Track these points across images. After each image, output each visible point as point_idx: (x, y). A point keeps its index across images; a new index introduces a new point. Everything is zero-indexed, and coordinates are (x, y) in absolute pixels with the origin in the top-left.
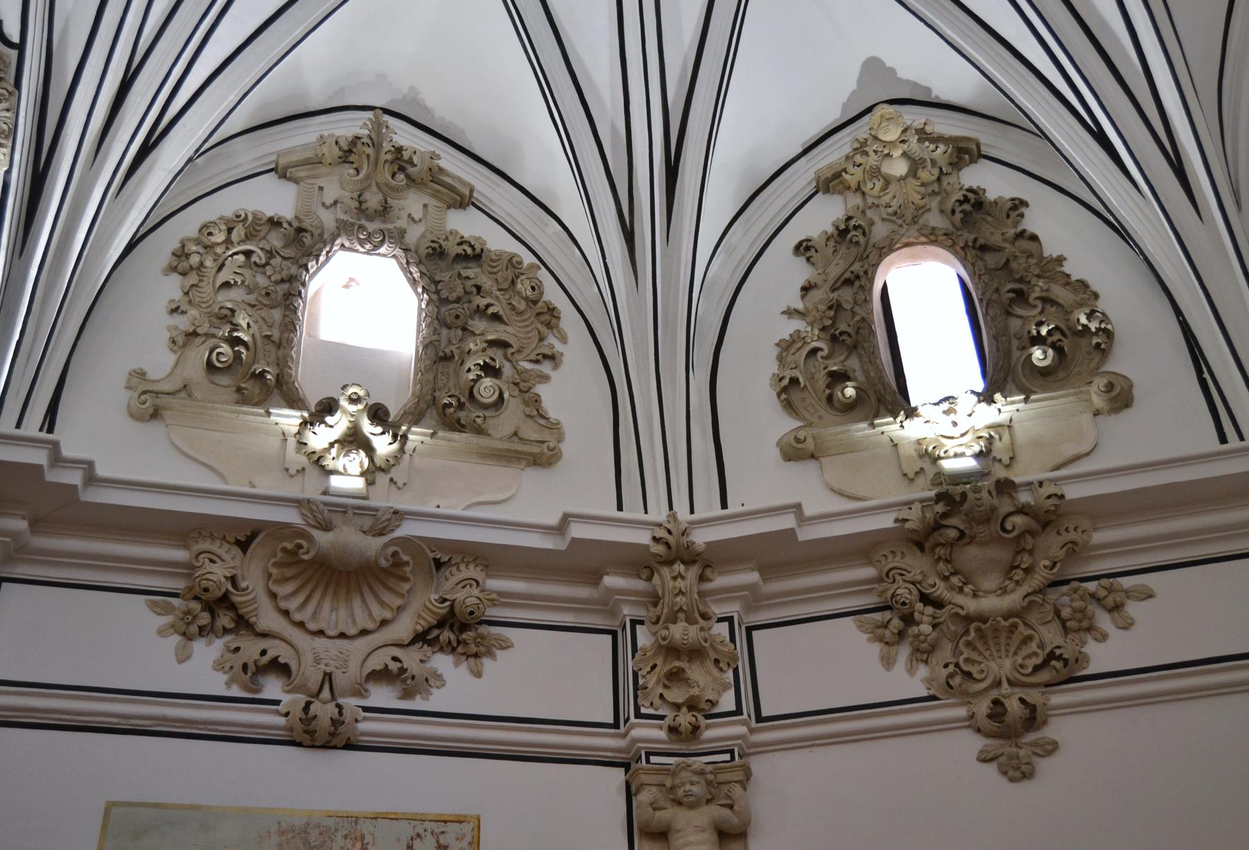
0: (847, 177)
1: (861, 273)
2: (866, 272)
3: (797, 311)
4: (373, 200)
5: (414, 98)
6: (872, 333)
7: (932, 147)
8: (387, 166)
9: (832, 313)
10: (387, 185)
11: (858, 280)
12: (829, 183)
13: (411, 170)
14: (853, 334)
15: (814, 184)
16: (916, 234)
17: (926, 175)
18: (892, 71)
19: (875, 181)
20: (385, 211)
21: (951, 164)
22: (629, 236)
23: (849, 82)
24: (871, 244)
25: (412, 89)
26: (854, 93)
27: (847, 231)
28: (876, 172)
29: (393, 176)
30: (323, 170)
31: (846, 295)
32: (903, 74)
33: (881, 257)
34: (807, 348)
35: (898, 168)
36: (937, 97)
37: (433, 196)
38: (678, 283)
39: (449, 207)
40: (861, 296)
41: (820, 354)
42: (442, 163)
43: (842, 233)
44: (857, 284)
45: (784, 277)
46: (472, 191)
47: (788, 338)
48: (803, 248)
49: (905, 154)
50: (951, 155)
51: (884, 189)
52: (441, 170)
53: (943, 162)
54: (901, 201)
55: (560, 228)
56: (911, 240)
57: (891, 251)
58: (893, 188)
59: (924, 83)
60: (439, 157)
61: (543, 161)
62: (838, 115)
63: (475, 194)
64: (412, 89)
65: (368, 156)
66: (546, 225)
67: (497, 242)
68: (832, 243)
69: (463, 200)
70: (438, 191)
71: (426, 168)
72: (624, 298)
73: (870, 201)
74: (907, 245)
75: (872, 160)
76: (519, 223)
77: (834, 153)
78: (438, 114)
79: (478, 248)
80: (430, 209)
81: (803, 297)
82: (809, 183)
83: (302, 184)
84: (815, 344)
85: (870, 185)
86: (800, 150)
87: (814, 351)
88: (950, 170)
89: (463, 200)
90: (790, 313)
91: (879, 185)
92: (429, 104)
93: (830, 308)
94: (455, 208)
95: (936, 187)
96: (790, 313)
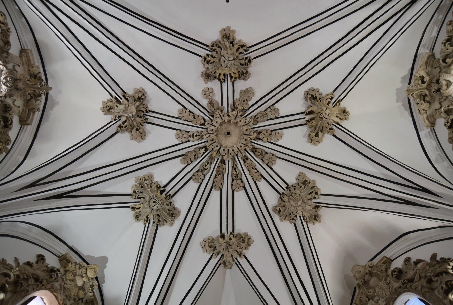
0: (70, 265)
1: (43, 283)
2: (43, 285)
3: (19, 263)
4: (20, 85)
5: (54, 104)
6: (24, 297)
7: (90, 291)
8: (32, 92)
9: (26, 277)
10: (26, 92)
11: (39, 284)
12: (64, 260)
13: (33, 101)
14: (21, 289)
15: (61, 255)
16: (63, 299)
17: (81, 294)
18: (105, 267)
19: (73, 275)
20: (17, 89)
21: (86, 301)
22: (33, 185)
23: (97, 254)
24: (52, 283)
25: (58, 103)
26: (93, 257)
27: (54, 271)
28: (75, 275)
29: (29, 94)
30: (26, 68)
31: (32, 281)
32: (106, 271)
33: (49, 289)
34: (9, 272)
35: (79, 282)
36: (103, 286)
37: (23, 110)
38: (21, 208)
39: (20, 116)
40: (35, 287)
41: (8, 278)
42: (37, 113)
43: (52, 270)
44: (38, 283)
45: (28, 254)
46: (29, 124)
47: (7, 263)
48: (41, 258)
49: (84, 282)
50: (90, 299)
51: (70, 280)
52: (34, 112)
53: (86, 298)
54: (70, 288)
55: (21, 160)
56: (59, 298)
57: (52, 292)
58: (73, 283)
59: (106, 279)
60: (39, 111)
61: (48, 150)
62: (85, 255)
63: (26, 126)
64: (58, 103)
65: (37, 84)
66: (21, 155)
67: (12, 134)
68: (46, 269)
69: (24, 122)
70: (26, 112)
71: (34, 106)
72: (10, 187)
73: (64, 277)
74: (57, 298)
75: (78, 272)
76: (19, 145)
77: (421, 119)
78: (51, 112)
79: (10, 126)
80: (18, 109)
81: (25, 264)
82: (61, 253)
83: (19, 59)
84: (12, 275)
85: (71, 274)
86: (71, 245)
87: (9, 276)
88: (84, 302)
89: (24, 122)
90: (16, 260)
91: (72, 278)
92: (54, 109)
93: (27, 276)
94: (20, 119)
95: (77, 300)
96: (16, 260)
